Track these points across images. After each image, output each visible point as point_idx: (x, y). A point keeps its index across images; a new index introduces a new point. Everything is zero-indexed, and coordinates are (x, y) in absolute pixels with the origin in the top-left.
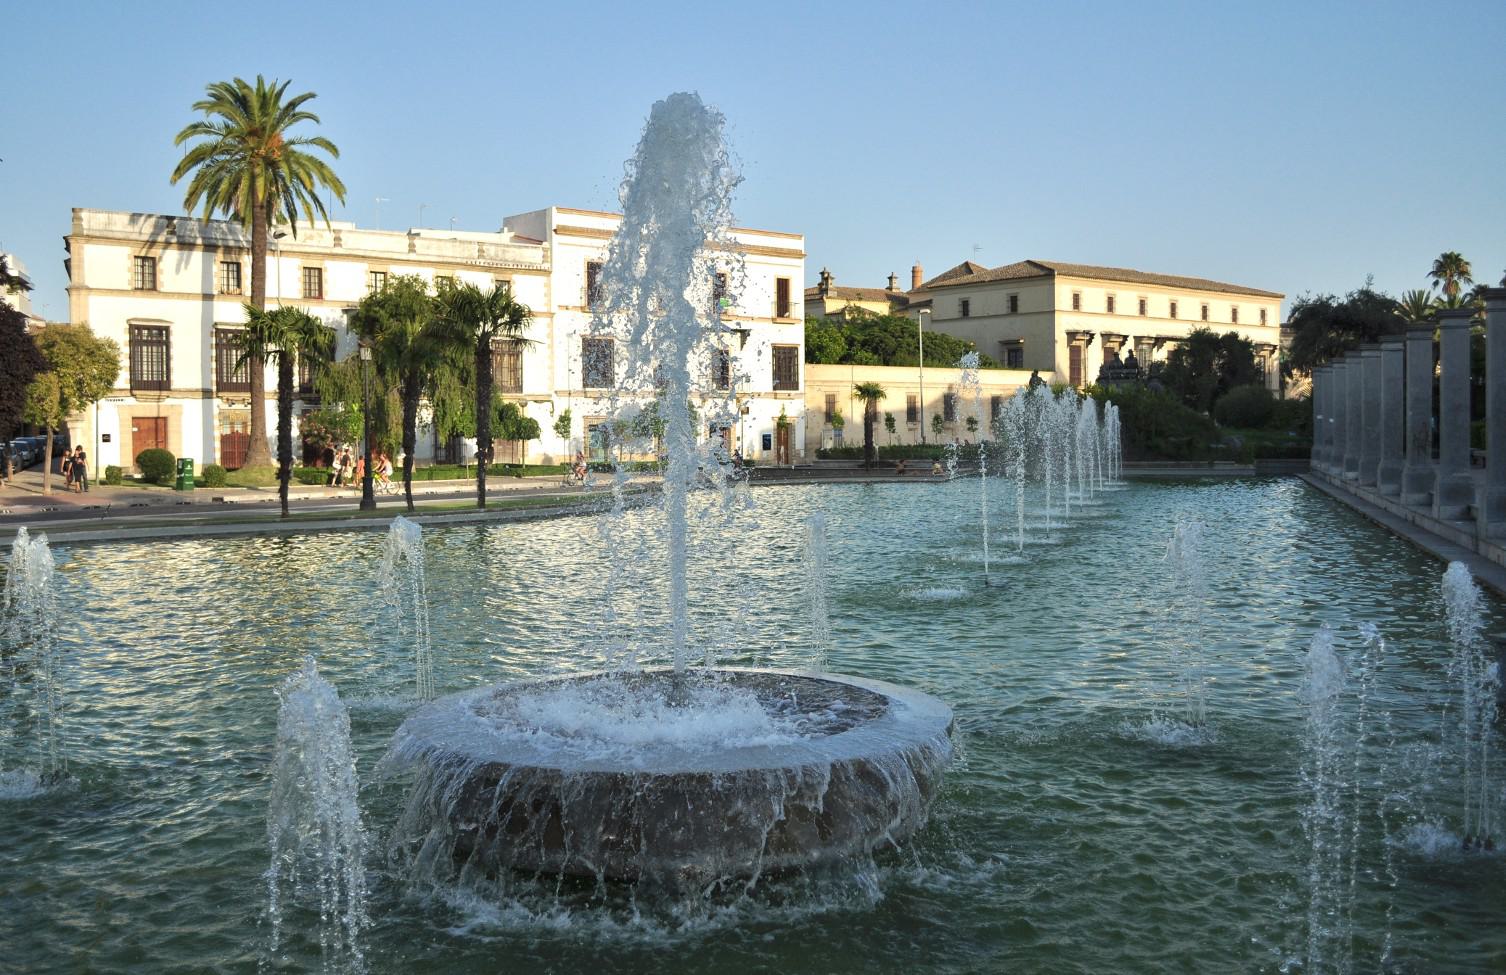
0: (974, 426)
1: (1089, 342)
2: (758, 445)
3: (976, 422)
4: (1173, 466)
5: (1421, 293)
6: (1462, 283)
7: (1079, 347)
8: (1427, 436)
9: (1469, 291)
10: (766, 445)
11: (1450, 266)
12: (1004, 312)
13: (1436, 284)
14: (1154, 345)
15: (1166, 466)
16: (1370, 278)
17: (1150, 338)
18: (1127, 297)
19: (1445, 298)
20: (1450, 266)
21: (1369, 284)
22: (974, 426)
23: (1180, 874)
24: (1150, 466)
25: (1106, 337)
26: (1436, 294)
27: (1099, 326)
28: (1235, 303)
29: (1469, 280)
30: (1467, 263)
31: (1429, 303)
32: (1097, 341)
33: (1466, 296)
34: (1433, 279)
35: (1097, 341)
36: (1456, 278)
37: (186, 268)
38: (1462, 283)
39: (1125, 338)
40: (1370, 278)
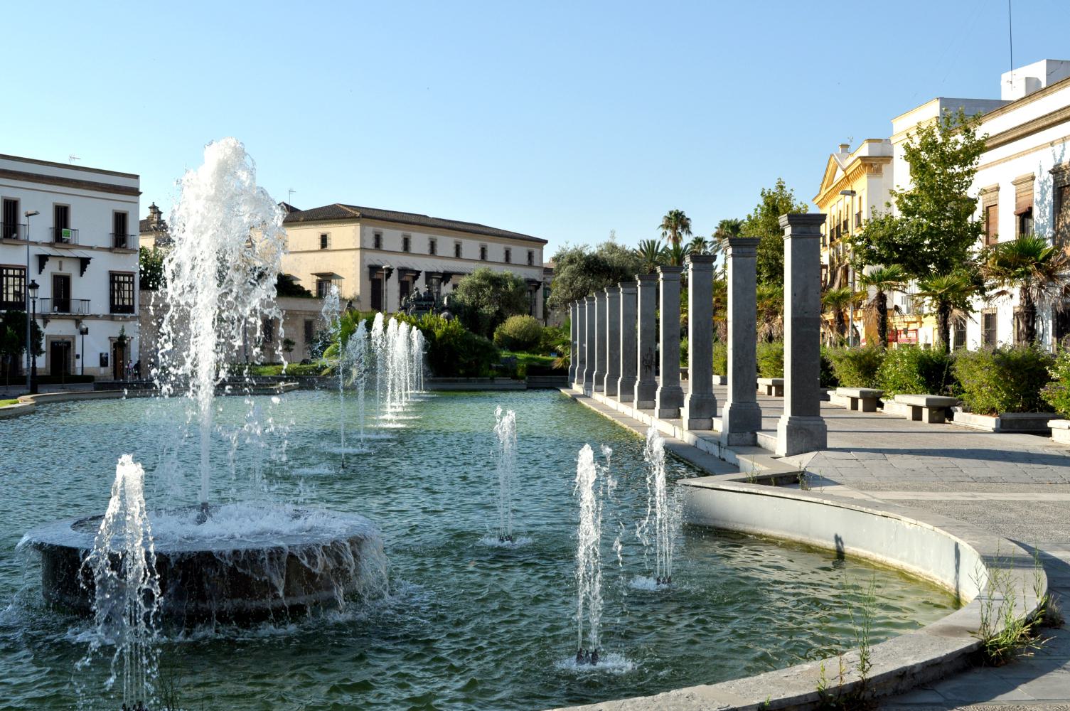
0: (291, 347)
1: (388, 276)
2: (97, 363)
3: (294, 344)
4: (463, 381)
5: (653, 243)
6: (684, 235)
7: (408, 282)
8: (652, 358)
9: (690, 241)
10: (103, 362)
11: (678, 221)
12: (316, 249)
13: (664, 234)
14: (441, 280)
15: (456, 381)
16: (613, 233)
17: (438, 273)
18: (420, 241)
19: (671, 247)
20: (678, 221)
21: (613, 236)
22: (291, 347)
23: (116, 650)
24: (444, 381)
25: (403, 271)
26: (666, 243)
27: (396, 262)
28: (433, 236)
29: (690, 232)
30: (688, 219)
31: (659, 251)
32: (395, 275)
33: (687, 246)
34: (662, 230)
35: (395, 275)
36: (680, 231)
37: (299, 280)
38: (684, 235)
39: (418, 273)
40: (613, 233)
